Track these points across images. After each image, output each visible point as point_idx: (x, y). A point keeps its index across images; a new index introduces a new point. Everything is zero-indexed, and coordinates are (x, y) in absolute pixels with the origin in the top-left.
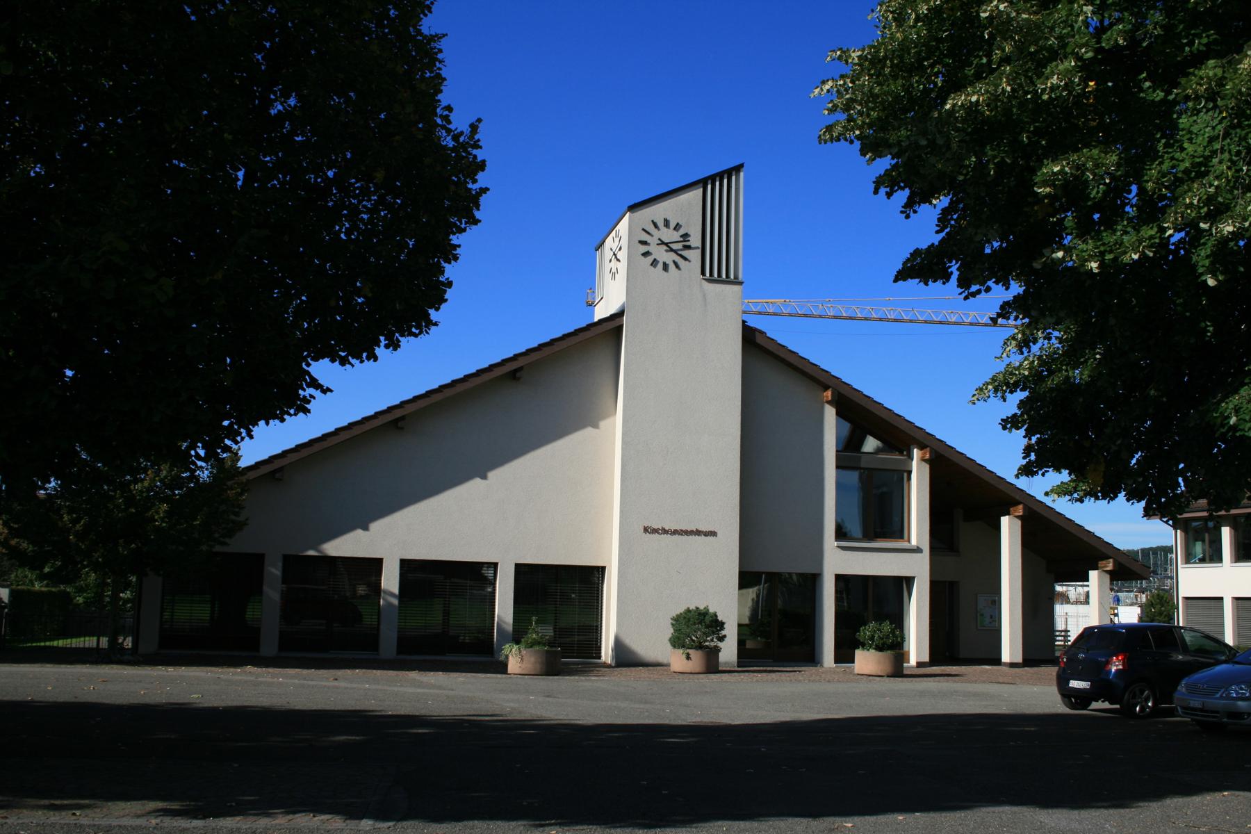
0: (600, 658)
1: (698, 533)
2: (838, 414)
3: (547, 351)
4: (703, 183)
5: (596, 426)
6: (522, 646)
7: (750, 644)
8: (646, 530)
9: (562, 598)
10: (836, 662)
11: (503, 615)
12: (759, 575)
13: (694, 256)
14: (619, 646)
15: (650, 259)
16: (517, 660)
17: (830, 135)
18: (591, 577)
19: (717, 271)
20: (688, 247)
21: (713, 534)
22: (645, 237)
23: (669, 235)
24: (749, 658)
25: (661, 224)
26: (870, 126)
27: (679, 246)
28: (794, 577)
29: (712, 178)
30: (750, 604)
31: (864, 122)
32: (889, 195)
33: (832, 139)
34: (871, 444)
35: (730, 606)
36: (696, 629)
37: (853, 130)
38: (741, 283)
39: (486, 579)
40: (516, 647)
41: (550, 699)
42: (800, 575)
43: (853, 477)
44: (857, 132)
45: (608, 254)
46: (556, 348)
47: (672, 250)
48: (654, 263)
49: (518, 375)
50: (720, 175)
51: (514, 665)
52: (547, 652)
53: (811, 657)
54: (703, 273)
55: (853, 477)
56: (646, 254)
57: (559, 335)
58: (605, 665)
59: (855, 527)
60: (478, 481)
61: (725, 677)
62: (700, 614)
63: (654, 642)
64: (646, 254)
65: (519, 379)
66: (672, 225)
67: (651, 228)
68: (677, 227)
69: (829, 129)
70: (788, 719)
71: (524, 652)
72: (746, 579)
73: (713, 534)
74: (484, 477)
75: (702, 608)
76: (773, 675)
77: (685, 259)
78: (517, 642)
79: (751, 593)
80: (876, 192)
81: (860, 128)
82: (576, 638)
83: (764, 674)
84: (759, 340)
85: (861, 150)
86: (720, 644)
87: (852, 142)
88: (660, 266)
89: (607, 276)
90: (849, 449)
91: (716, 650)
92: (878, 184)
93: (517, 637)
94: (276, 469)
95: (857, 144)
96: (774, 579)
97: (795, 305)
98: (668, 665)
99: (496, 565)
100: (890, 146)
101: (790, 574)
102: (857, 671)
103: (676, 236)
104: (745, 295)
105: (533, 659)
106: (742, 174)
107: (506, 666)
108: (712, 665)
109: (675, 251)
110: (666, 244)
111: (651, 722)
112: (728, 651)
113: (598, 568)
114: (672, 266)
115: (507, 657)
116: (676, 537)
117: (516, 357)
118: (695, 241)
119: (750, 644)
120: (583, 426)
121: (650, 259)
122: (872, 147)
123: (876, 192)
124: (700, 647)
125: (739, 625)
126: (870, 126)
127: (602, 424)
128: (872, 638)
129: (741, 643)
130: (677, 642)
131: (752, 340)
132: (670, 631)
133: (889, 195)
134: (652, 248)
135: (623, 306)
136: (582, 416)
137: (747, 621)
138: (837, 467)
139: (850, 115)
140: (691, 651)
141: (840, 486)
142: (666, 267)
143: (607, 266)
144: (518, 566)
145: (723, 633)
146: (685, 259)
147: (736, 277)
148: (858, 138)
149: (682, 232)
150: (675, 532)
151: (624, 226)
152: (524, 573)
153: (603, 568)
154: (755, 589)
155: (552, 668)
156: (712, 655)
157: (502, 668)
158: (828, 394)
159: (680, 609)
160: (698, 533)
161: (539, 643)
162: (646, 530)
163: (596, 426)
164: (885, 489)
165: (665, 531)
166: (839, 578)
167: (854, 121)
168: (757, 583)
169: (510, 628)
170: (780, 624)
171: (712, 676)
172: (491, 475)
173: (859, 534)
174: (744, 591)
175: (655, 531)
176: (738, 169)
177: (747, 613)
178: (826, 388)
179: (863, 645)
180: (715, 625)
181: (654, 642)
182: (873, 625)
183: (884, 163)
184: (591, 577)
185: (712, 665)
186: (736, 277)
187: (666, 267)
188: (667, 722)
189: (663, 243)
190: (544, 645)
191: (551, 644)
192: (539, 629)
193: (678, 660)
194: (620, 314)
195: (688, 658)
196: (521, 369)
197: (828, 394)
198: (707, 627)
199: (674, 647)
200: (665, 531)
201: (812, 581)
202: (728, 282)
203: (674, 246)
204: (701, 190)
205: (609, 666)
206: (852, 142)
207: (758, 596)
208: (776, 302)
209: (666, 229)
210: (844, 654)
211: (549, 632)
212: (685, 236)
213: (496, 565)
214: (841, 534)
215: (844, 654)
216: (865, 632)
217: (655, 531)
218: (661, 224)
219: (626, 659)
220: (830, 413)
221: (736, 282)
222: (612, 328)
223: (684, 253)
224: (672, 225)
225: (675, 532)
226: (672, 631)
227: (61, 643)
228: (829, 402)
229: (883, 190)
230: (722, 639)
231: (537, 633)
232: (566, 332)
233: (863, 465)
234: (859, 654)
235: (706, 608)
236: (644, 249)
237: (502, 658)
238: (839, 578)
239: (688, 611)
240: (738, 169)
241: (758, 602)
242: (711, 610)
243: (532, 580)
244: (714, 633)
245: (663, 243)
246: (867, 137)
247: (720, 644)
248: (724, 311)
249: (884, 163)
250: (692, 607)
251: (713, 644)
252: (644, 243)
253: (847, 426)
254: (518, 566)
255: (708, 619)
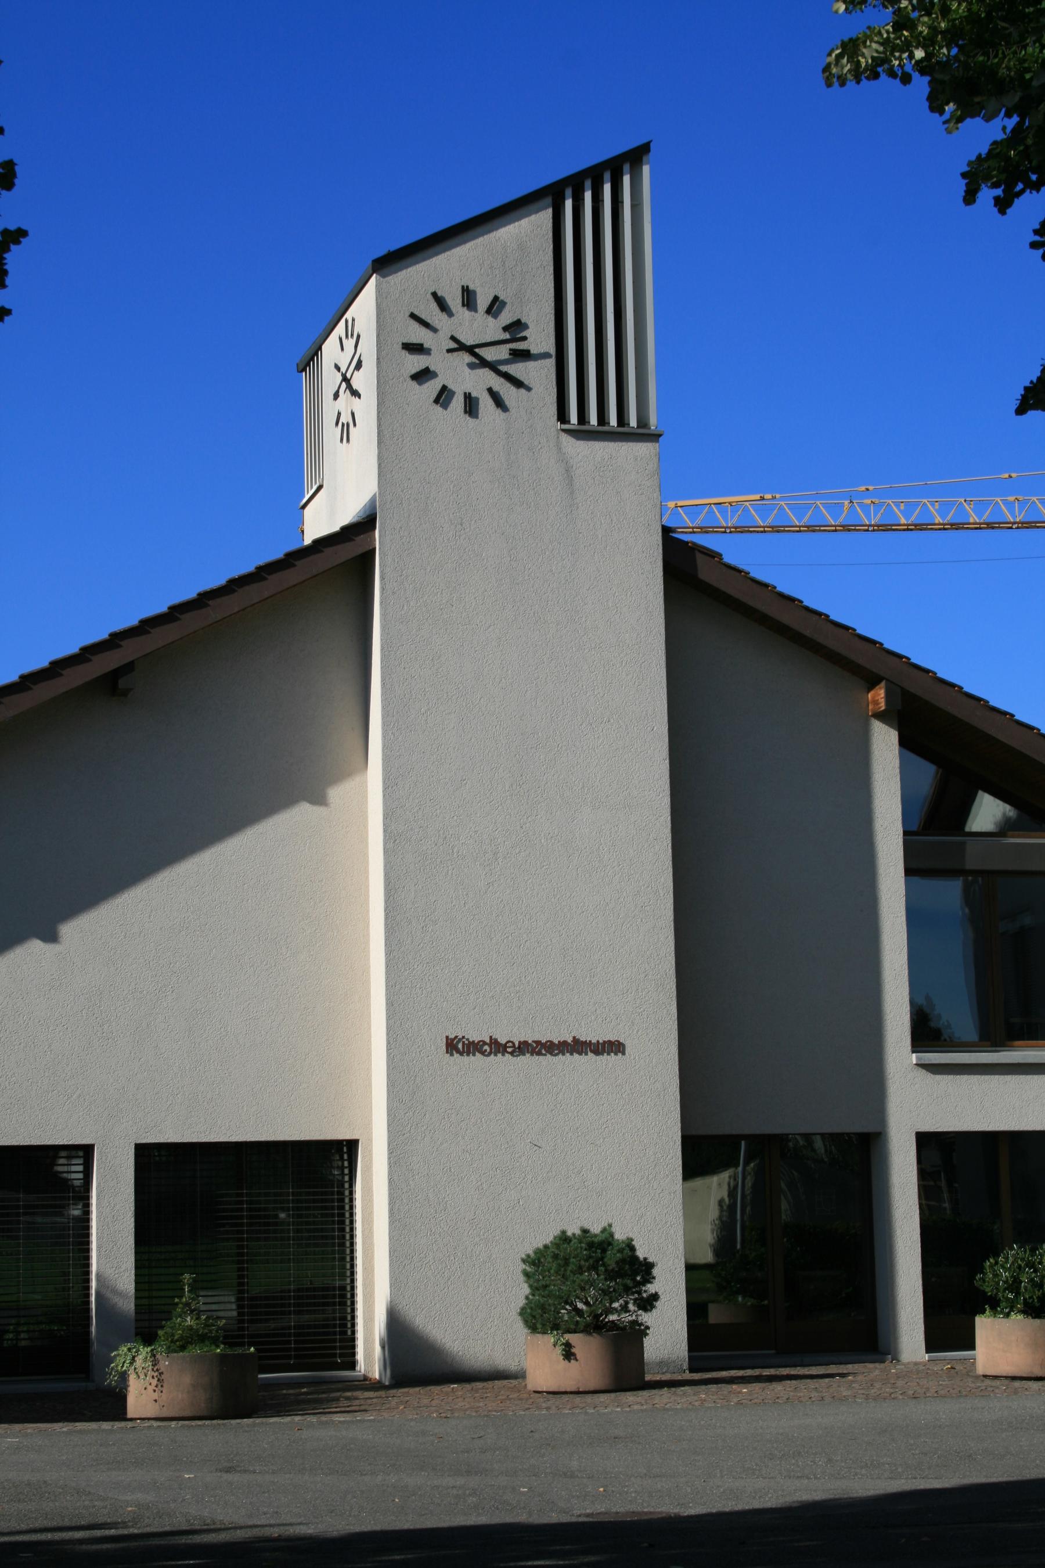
0: (352, 1365)
1: (578, 1047)
2: (904, 743)
3: (191, 622)
4: (552, 195)
5: (319, 799)
6: (160, 1348)
7: (716, 1315)
8: (451, 1046)
9: (253, 1217)
10: (928, 1350)
11: (110, 1273)
12: (731, 1142)
13: (539, 374)
14: (399, 1333)
15: (432, 387)
16: (149, 1384)
17: (855, 65)
18: (322, 1170)
19: (596, 413)
20: (524, 355)
21: (615, 1047)
22: (418, 334)
23: (479, 328)
24: (716, 1348)
25: (454, 301)
26: (952, 36)
27: (500, 353)
28: (819, 1144)
29: (575, 183)
30: (713, 1212)
31: (934, 29)
32: (1003, 205)
33: (857, 74)
34: (987, 812)
35: (663, 1221)
36: (583, 1282)
37: (907, 47)
38: (655, 437)
39: (62, 1185)
40: (144, 1351)
41: (234, 1477)
42: (834, 1139)
43: (950, 894)
44: (919, 54)
45: (330, 380)
46: (214, 613)
47: (484, 363)
48: (443, 397)
49: (122, 683)
50: (594, 175)
51: (141, 1397)
52: (223, 1357)
53: (865, 1336)
54: (562, 416)
55: (950, 894)
56: (422, 376)
57: (218, 581)
58: (367, 1384)
59: (958, 1014)
60: (36, 946)
61: (662, 1397)
62: (591, 1245)
63: (485, 1321)
64: (422, 376)
65: (125, 693)
66: (483, 302)
67: (431, 312)
68: (495, 307)
69: (851, 48)
70: (818, 1496)
71: (164, 1363)
72: (699, 1155)
73: (615, 1047)
74: (51, 937)
75: (596, 1229)
76: (778, 1387)
77: (518, 383)
78: (148, 1338)
79: (716, 1186)
80: (970, 197)
81: (927, 43)
82: (293, 1320)
83: (757, 1387)
84: (706, 573)
85: (931, 98)
86: (645, 1318)
87: (906, 79)
88: (458, 403)
89: (331, 433)
90: (935, 827)
91: (637, 1333)
92: (974, 179)
93: (146, 1328)
94: (268, 1385)
95: (921, 84)
96: (769, 1149)
97: (786, 508)
98: (520, 1375)
99: (86, 1152)
100: (1001, 88)
101: (807, 1137)
102: (980, 1370)
103: (492, 329)
104: (669, 483)
105: (187, 1379)
106: (646, 169)
107: (120, 1398)
108: (628, 1372)
109: (493, 366)
110: (470, 350)
111: (483, 1520)
112: (666, 1332)
113: (339, 1144)
114: (486, 404)
115: (124, 1376)
116: (526, 1059)
117: (116, 640)
118: (540, 338)
119: (716, 1315)
120: (287, 801)
121: (432, 387)
122: (958, 90)
123: (970, 197)
124: (596, 1326)
125: (690, 1268)
126: (952, 36)
127: (335, 794)
128: (1014, 1285)
129: (695, 1311)
130: (539, 1317)
131: (689, 574)
132: (520, 1292)
133: (1003, 205)
134: (438, 360)
135: (372, 502)
136: (288, 775)
137: (707, 1256)
138: (909, 872)
139: (898, 12)
140: (573, 1338)
141: (915, 917)
142: (471, 406)
143: (330, 409)
144: (143, 1151)
145: (651, 1288)
146: (518, 383)
147: (643, 422)
148: (922, 67)
149: (506, 317)
150: (523, 1048)
151: (364, 309)
152: (151, 1159)
153: (352, 1145)
154: (725, 1176)
155: (235, 1399)
156: (627, 1341)
157: (111, 1404)
158: (879, 696)
159: (545, 1237)
160: (578, 1047)
161: (202, 1339)
162: (451, 1046)
163: (319, 799)
164: (1027, 920)
165: (497, 1047)
166: (925, 1141)
167: (911, 25)
168: (730, 1162)
169: (128, 1305)
170: (789, 1269)
171: (630, 1397)
172: (68, 930)
173: (973, 1036)
174: (698, 1183)
175: (472, 1048)
176: (636, 156)
177: (708, 1235)
178: (872, 681)
179: (993, 1304)
180: (631, 1271)
181: (485, 1321)
182: (1014, 1253)
183: (983, 133)
184: (322, 1170)
185: (628, 1372)
186: (643, 422)
187: (471, 406)
188: (522, 1518)
189: (461, 347)
190: (215, 1342)
191: (231, 1338)
192: (201, 1303)
193: (543, 1363)
194: (366, 524)
195: (569, 1354)
196: (129, 668)
197: (879, 696)
198: (611, 1275)
199: (533, 1329)
200: (497, 1047)
201: (865, 1149)
202: (623, 434)
203: (489, 354)
204: (549, 212)
205: (377, 1386)
206: (906, 79)
207: (732, 1193)
208: (744, 502)
209: (465, 314)
210: (949, 1331)
211: (225, 1307)
212: (516, 328)
213: (86, 1152)
214: (926, 1033)
215: (949, 1331)
216: (998, 1272)
217: (472, 1048)
218: (454, 301)
219: (416, 1363)
220: (885, 743)
221: (644, 434)
222: (350, 555)
223: (517, 369)
224: (483, 302)
225: (523, 1048)
226: (526, 1290)
227: (592, 1558)
228: (881, 716)
229: (987, 195)
230: (648, 1303)
231: (197, 1313)
232: (235, 574)
233: (971, 864)
234: (985, 1326)
235: (607, 1231)
236: (417, 363)
237: (113, 1380)
238: (925, 1141)
239: (564, 1238)
240: (636, 156)
241: (732, 1207)
242: (620, 1235)
243: (171, 1175)
244: (627, 1290)
245: (461, 347)
246: (945, 65)
247: (645, 1318)
248: (613, 511)
249: (983, 133)
250: (573, 1230)
251: (627, 1318)
252: (415, 348)
253: (927, 772)
254: (143, 1151)
255: (612, 1258)
